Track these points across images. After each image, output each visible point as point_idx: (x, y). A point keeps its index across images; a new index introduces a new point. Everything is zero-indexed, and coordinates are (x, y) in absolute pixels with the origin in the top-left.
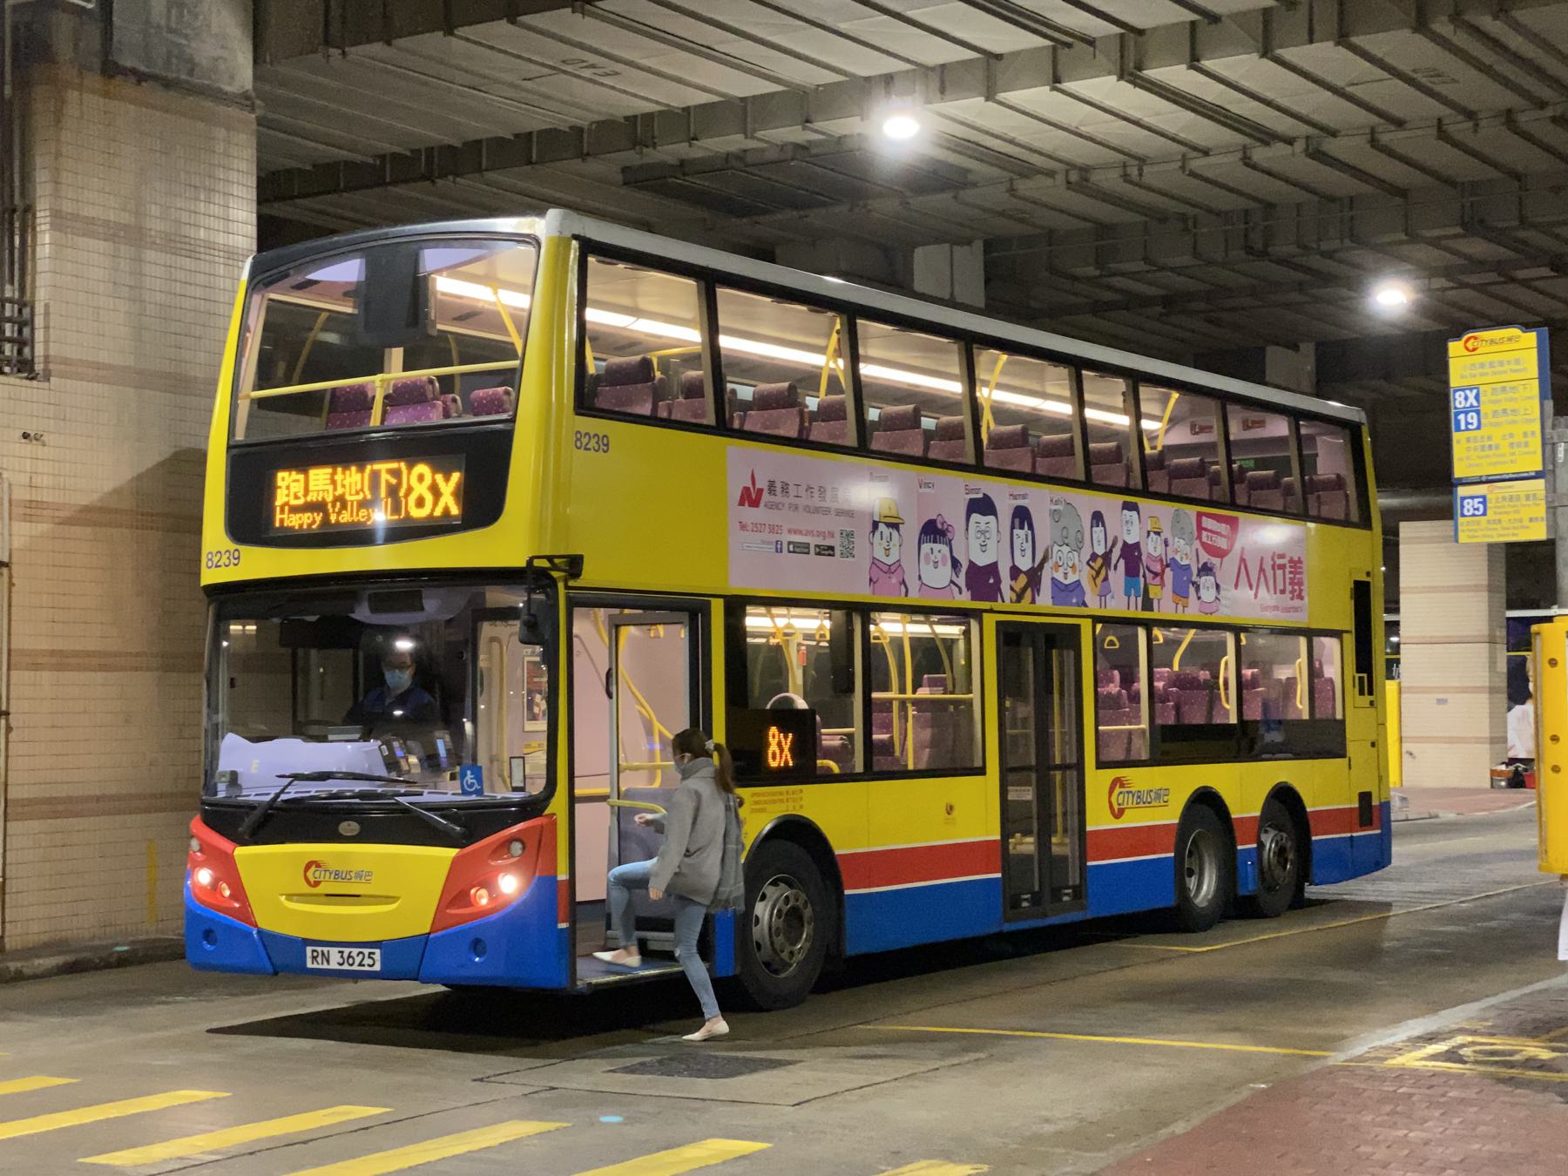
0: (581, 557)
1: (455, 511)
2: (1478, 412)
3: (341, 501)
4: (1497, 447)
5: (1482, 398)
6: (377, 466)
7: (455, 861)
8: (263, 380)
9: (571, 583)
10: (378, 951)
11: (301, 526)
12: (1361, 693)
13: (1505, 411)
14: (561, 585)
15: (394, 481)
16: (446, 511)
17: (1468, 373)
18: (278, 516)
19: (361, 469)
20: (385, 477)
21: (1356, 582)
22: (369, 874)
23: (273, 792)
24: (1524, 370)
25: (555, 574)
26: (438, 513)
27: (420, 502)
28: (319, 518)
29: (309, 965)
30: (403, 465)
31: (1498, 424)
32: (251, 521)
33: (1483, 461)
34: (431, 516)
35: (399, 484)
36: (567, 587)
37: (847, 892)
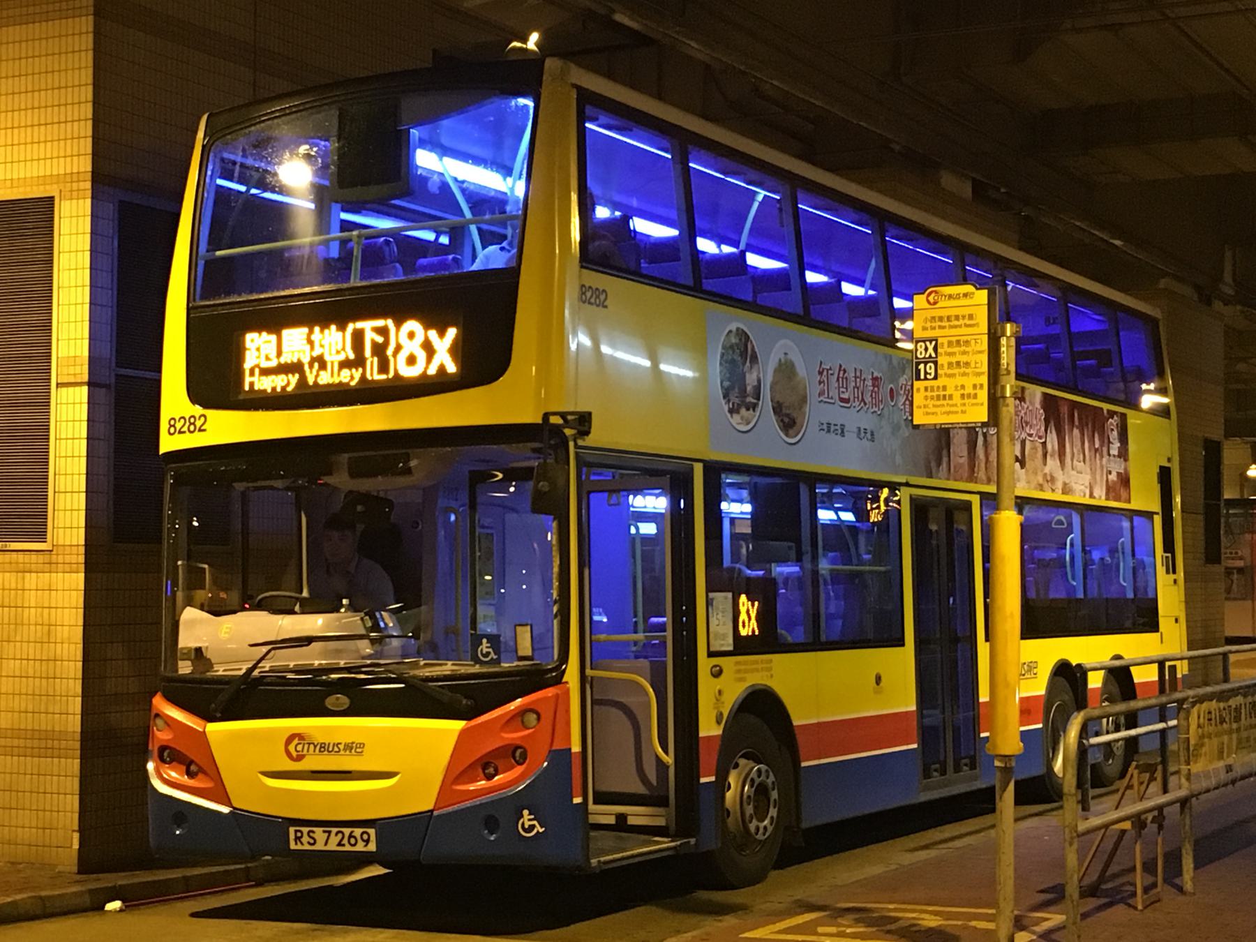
0: (590, 414)
1: (452, 368)
2: (936, 363)
3: (321, 362)
4: (951, 397)
5: (939, 350)
6: (359, 325)
7: (463, 733)
8: (215, 244)
9: (580, 443)
10: (372, 832)
11: (274, 389)
12: (1168, 572)
13: (958, 363)
14: (571, 444)
15: (380, 339)
16: (442, 369)
17: (929, 325)
18: (248, 380)
19: (342, 328)
20: (370, 337)
21: (1161, 467)
22: (362, 745)
23: (244, 668)
24: (976, 325)
25: (568, 432)
26: (432, 371)
27: (411, 360)
28: (294, 379)
29: (293, 846)
30: (390, 323)
31: (952, 376)
32: (216, 383)
33: (938, 410)
34: (424, 375)
35: (387, 343)
36: (576, 446)
37: (804, 764)
